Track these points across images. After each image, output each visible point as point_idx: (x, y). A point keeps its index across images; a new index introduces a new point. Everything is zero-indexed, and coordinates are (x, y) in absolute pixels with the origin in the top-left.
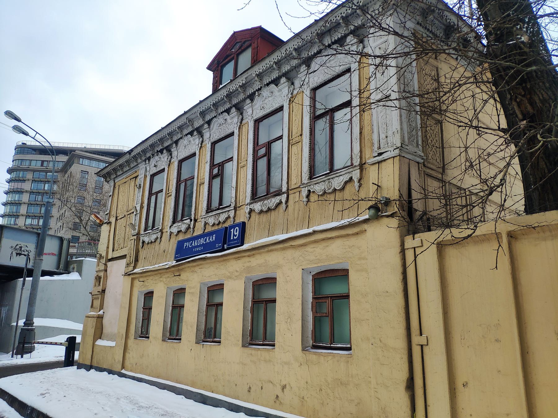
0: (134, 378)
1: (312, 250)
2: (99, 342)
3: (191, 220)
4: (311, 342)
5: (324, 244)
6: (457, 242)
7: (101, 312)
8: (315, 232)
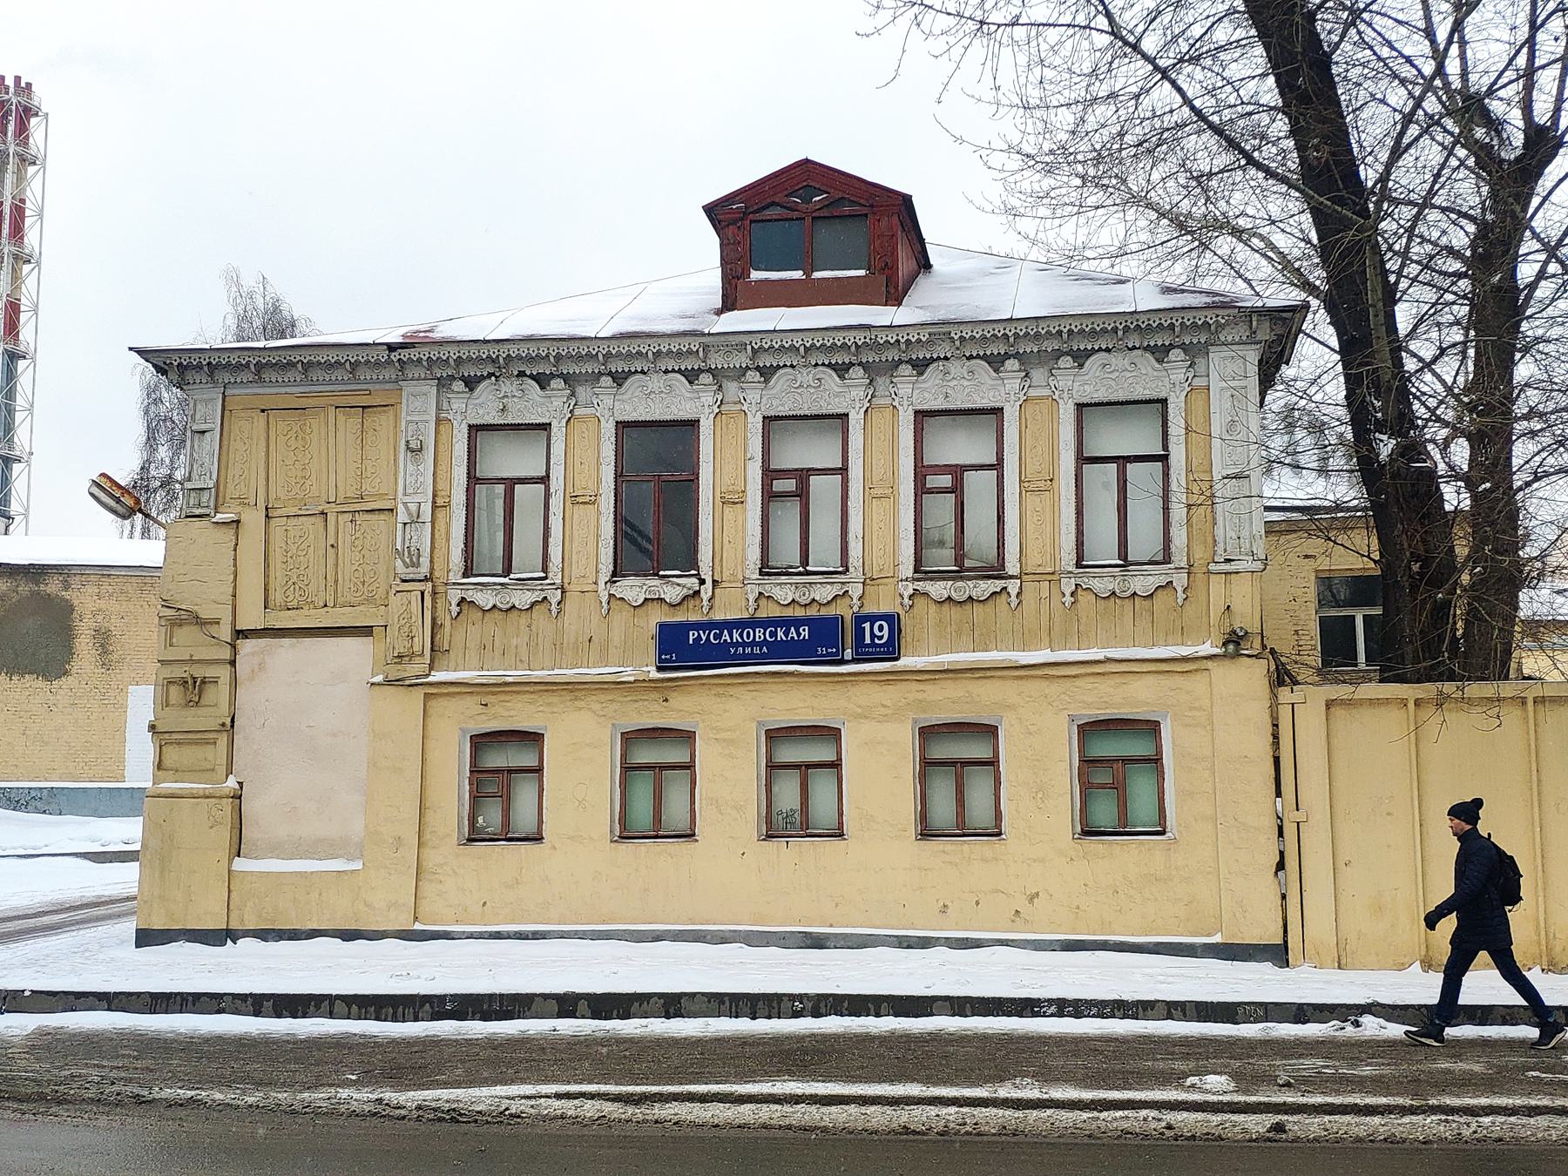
0: (471, 936)
1: (1090, 686)
2: (240, 864)
3: (702, 582)
4: (1079, 829)
5: (1118, 679)
6: (1348, 703)
7: (232, 782)
8: (1109, 660)
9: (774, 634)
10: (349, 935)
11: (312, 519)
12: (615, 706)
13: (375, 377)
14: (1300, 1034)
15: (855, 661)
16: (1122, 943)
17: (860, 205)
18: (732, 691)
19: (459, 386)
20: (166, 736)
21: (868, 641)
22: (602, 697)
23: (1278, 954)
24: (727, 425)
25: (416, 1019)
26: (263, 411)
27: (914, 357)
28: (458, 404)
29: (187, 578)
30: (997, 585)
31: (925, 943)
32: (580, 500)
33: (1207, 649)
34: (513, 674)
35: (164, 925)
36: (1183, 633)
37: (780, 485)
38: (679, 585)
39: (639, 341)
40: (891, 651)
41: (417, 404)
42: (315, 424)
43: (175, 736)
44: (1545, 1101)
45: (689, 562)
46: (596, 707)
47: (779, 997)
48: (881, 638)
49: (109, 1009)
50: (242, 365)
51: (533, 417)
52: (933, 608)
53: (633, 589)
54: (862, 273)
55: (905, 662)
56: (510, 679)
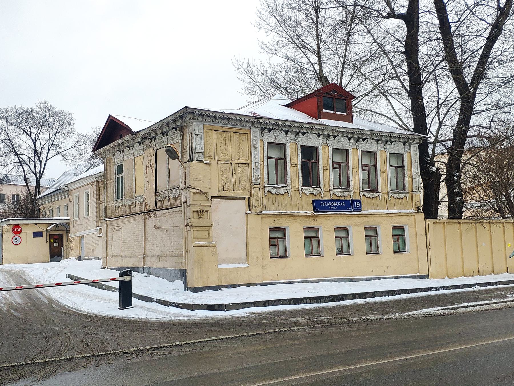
0: (277, 283)
1: (394, 219)
3: (322, 190)
5: (399, 217)
9: (337, 204)
10: (248, 285)
11: (228, 164)
12: (304, 221)
13: (246, 125)
14: (461, 291)
15: (354, 211)
16: (404, 276)
17: (344, 97)
18: (328, 218)
19: (361, 140)
20: (195, 228)
21: (356, 207)
22: (301, 219)
23: (427, 276)
24: (324, 149)
25: (325, 302)
26: (215, 131)
27: (269, 128)
28: (265, 136)
29: (197, 180)
30: (376, 194)
31: (371, 279)
32: (293, 165)
33: (412, 211)
34: (283, 212)
35: (202, 285)
36: (407, 207)
37: (336, 166)
38: (317, 190)
39: (313, 125)
40: (360, 209)
41: (255, 134)
42: (228, 136)
43: (198, 228)
44: (495, 301)
45: (318, 184)
46: (299, 221)
47: (392, 291)
48: (358, 206)
49: (254, 307)
50: (224, 118)
51: (282, 141)
52: (366, 199)
53: (307, 190)
54: (345, 114)
55: (363, 212)
56: (283, 213)
